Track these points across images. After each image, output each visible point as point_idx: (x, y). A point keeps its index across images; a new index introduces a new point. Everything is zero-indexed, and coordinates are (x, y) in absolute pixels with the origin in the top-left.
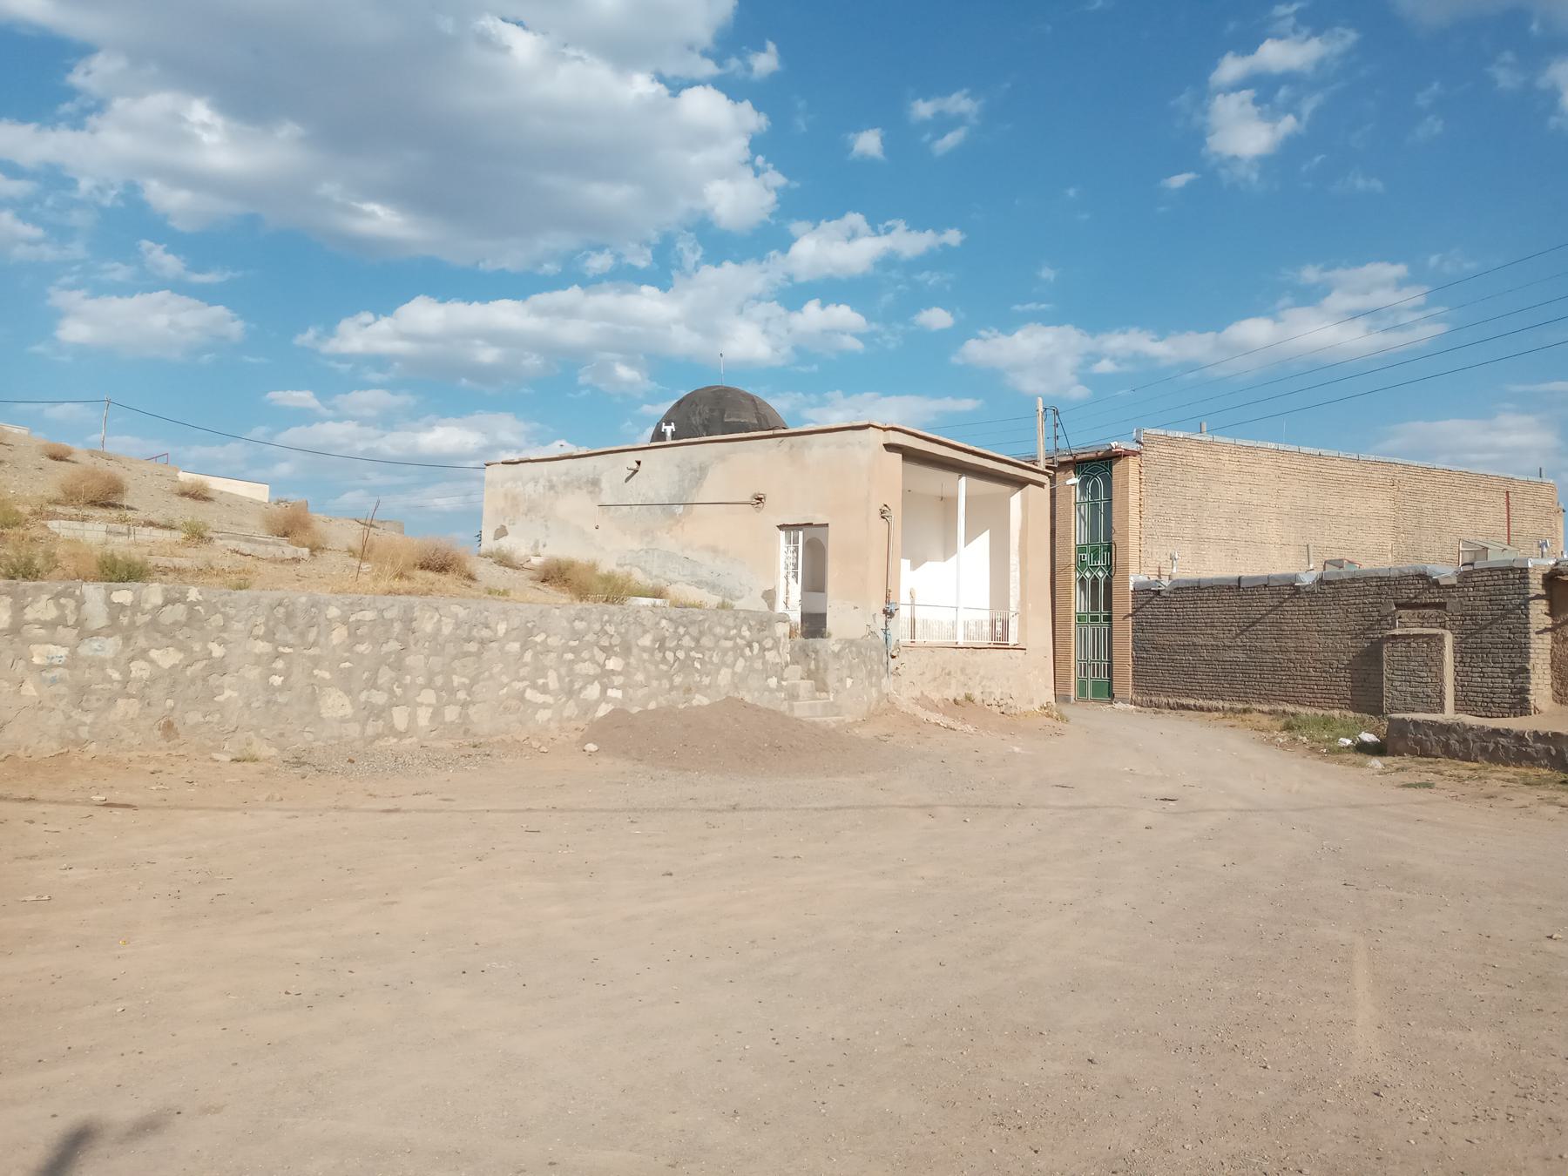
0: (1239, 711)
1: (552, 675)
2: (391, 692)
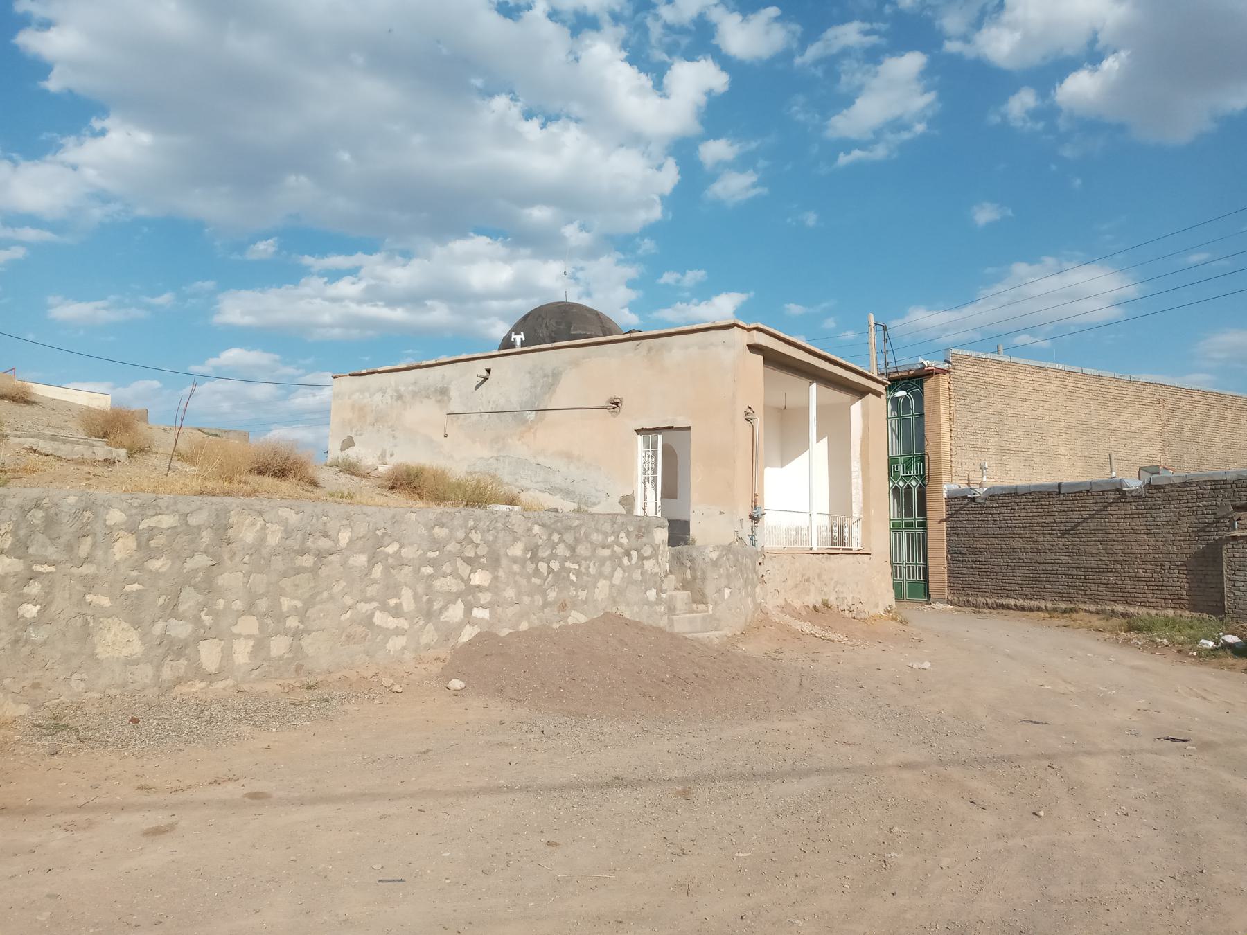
0: (1065, 611)
1: (406, 593)
2: (197, 620)
